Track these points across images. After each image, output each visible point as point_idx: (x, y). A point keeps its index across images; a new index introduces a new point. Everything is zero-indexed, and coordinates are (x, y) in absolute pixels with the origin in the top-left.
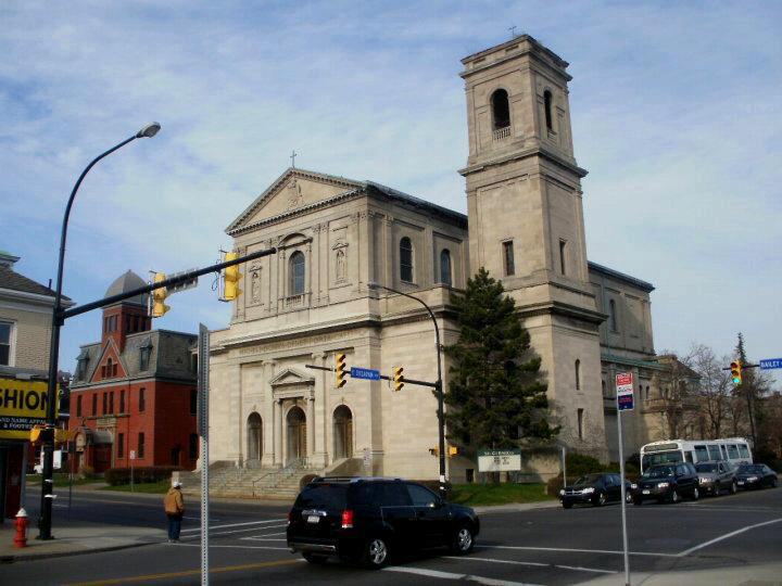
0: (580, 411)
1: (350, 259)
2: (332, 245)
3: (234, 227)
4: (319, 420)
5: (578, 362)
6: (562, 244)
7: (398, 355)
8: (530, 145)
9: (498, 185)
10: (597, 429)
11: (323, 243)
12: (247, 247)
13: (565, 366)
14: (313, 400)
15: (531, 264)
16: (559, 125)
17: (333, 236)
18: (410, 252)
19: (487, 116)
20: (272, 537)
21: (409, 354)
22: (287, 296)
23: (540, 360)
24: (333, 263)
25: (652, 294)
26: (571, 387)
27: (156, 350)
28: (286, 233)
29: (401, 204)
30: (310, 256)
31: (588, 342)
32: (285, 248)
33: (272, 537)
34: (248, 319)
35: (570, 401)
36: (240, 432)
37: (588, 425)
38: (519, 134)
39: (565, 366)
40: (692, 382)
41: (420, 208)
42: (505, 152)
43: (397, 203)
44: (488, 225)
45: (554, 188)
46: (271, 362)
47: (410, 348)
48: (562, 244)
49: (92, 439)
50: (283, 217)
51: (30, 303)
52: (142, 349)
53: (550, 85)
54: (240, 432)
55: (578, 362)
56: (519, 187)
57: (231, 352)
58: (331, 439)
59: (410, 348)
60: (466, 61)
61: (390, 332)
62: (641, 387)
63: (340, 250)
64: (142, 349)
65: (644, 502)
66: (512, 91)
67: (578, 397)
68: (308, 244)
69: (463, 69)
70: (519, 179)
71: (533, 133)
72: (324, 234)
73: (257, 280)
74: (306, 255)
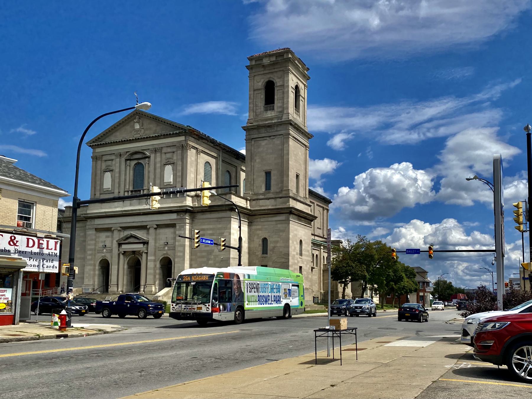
3: (94, 142)
4: (151, 265)
9: (265, 138)
11: (158, 159)
12: (102, 155)
14: (147, 253)
19: (261, 96)
21: (210, 229)
22: (131, 189)
26: (297, 254)
28: (132, 151)
30: (149, 167)
31: (306, 231)
32: (130, 160)
40: (360, 259)
43: (204, 141)
44: (257, 161)
47: (211, 227)
50: (138, 139)
51: (37, 191)
57: (89, 220)
59: (211, 227)
60: (250, 59)
62: (313, 254)
65: (243, 291)
67: (299, 260)
68: (147, 159)
69: (248, 63)
72: (158, 154)
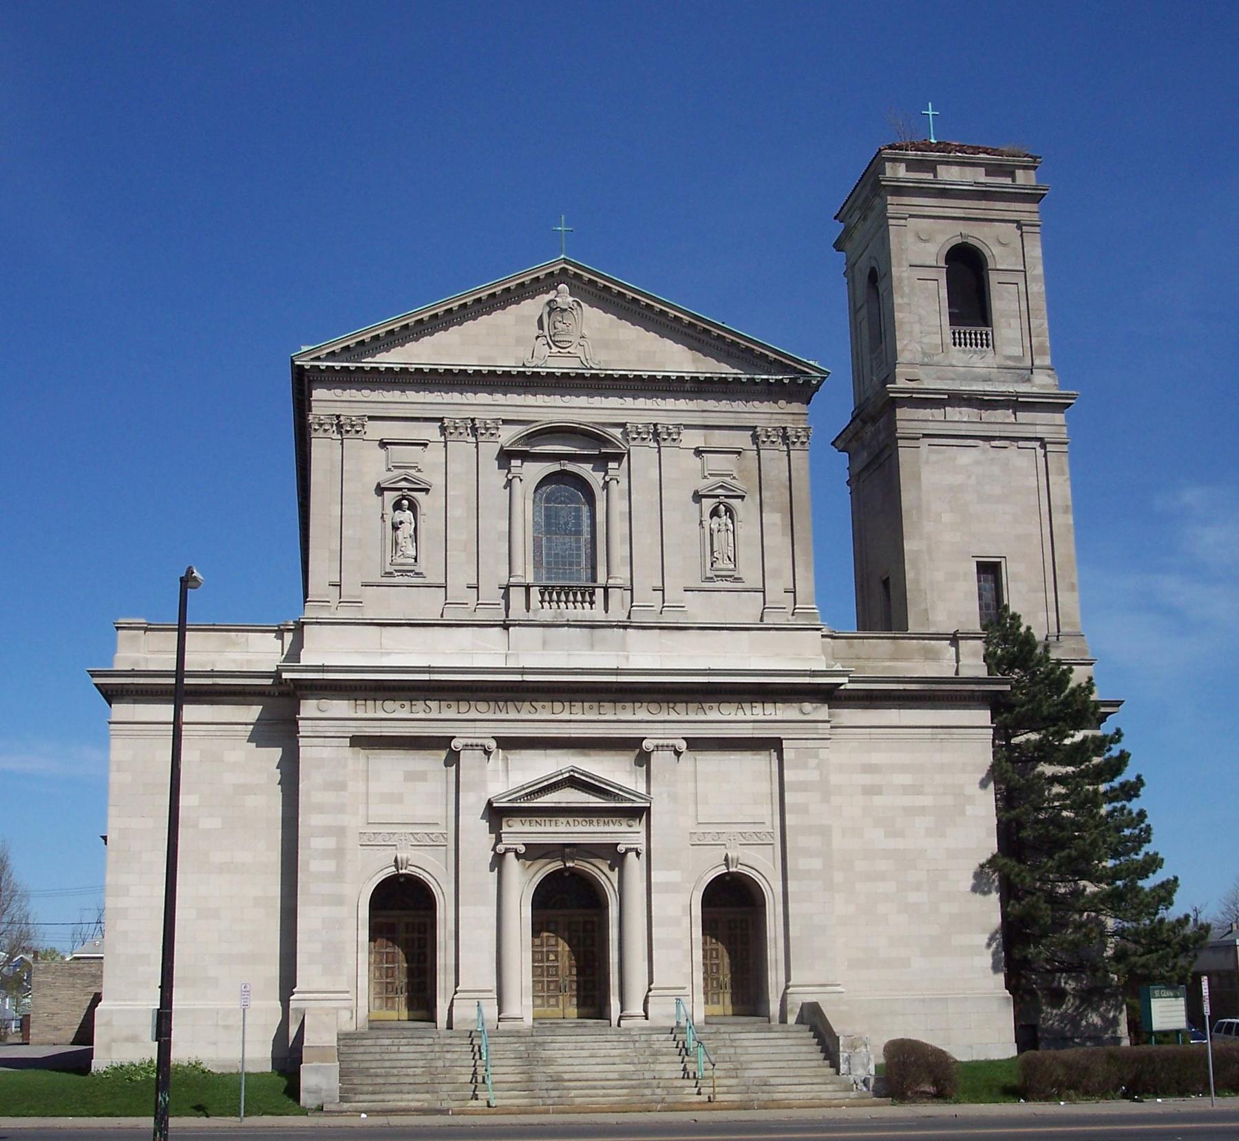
70: (1021, 444)
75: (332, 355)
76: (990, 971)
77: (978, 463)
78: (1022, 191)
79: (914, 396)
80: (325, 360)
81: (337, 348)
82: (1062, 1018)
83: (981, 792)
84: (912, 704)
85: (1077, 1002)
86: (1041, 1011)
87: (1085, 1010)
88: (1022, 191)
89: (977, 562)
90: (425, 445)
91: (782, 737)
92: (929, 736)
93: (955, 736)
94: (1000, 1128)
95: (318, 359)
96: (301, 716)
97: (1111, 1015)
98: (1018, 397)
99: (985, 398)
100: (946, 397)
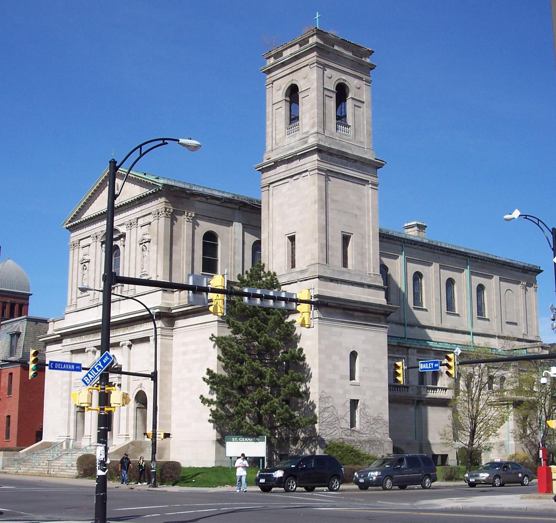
0: (354, 403)
1: (151, 253)
2: (139, 238)
5: (353, 355)
6: (346, 239)
7: (184, 344)
8: (312, 141)
10: (376, 420)
13: (335, 358)
15: (308, 257)
16: (354, 115)
17: (141, 231)
18: (216, 246)
20: (328, 502)
23: (121, 366)
24: (139, 258)
25: (538, 277)
26: (342, 377)
27: (23, 337)
29: (203, 199)
33: (328, 502)
34: (79, 307)
35: (340, 391)
36: (69, 415)
37: (364, 415)
38: (305, 130)
39: (335, 358)
41: (225, 202)
42: (293, 148)
45: (333, 180)
46: (93, 349)
48: (346, 239)
49: (204, 399)
52: (12, 335)
53: (344, 77)
54: (69, 415)
55: (353, 355)
56: (302, 181)
58: (132, 422)
61: (180, 323)
63: (144, 243)
64: (12, 335)
66: (302, 86)
70: (303, 175)
71: (315, 130)
73: (86, 271)
74: (121, 248)
75: (70, 222)
76: (213, 429)
77: (289, 189)
78: (307, 49)
79: (263, 167)
80: (69, 224)
81: (70, 219)
82: (297, 450)
83: (214, 350)
84: (198, 314)
85: (302, 443)
86: (290, 447)
87: (304, 447)
88: (307, 49)
89: (288, 237)
90: (89, 245)
91: (149, 336)
92: (200, 328)
93: (207, 327)
94: (451, 514)
95: (67, 224)
96: (47, 351)
97: (313, 450)
98: (296, 153)
99: (286, 158)
100: (273, 163)
